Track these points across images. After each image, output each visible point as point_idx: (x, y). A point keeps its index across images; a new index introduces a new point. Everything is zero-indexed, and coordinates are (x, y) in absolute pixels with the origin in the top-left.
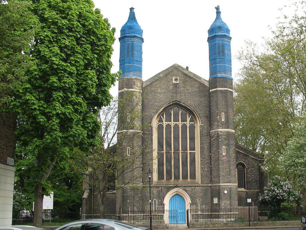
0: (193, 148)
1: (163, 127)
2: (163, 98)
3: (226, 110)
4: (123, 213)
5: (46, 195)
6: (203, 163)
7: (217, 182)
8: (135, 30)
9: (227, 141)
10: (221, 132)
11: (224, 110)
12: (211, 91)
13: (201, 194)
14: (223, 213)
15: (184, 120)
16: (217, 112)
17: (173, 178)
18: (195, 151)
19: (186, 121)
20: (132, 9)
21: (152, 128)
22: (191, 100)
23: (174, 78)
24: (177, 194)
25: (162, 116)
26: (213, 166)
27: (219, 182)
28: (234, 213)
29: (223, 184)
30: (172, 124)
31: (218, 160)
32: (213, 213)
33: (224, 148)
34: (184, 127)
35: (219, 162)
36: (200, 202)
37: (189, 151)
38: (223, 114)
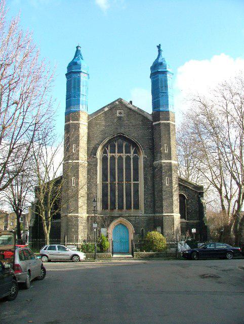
0: (136, 178)
19: (130, 153)
22: (134, 134)
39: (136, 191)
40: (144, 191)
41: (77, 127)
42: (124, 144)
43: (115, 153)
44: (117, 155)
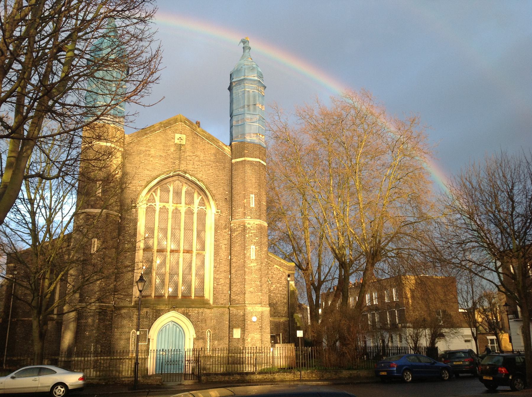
2: (157, 165)
4: (78, 354)
11: (254, 191)
15: (190, 202)
25: (154, 192)
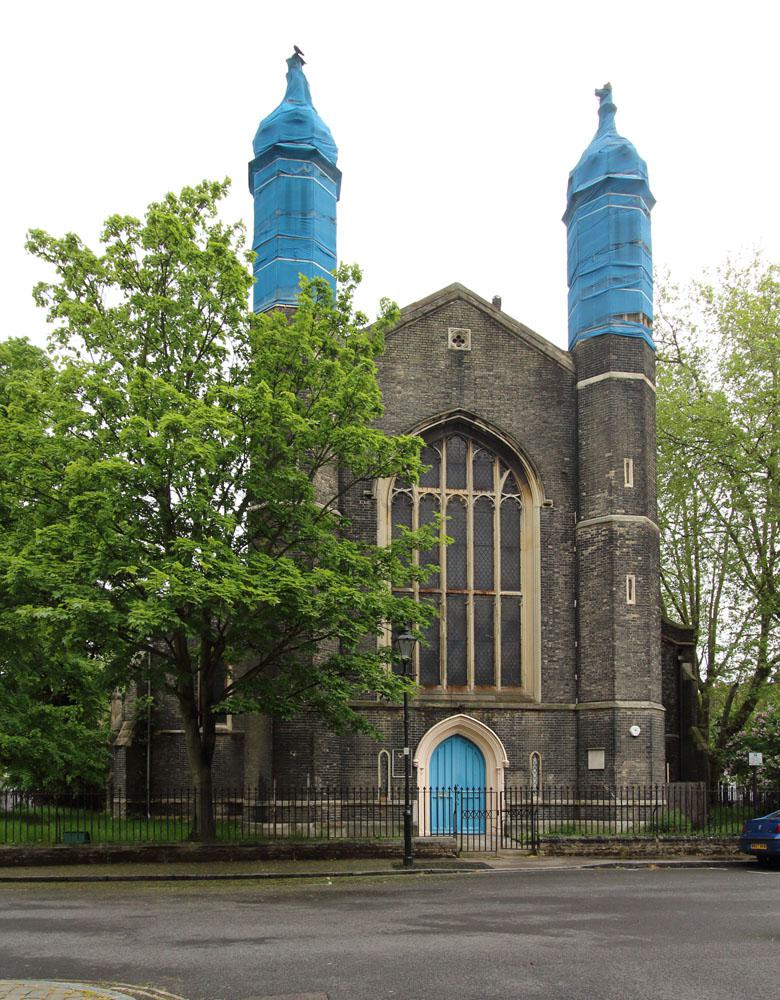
0: (513, 581)
1: (412, 505)
3: (640, 450)
5: (489, 319)
6: (550, 632)
7: (603, 698)
8: (313, 130)
9: (640, 558)
10: (622, 525)
12: (581, 384)
13: (544, 738)
14: (624, 803)
16: (607, 455)
17: (445, 682)
18: (518, 593)
19: (491, 488)
20: (296, 61)
21: (374, 502)
22: (512, 416)
23: (451, 333)
24: (457, 736)
26: (586, 642)
27: (611, 698)
28: (648, 802)
29: (627, 704)
30: (444, 494)
31: (609, 621)
32: (583, 801)
33: (630, 581)
34: (485, 505)
35: (613, 630)
36: (538, 762)
37: (499, 592)
38: (628, 464)
39: (513, 626)
40: (544, 624)
41: (382, 765)
42: (471, 456)
43: (438, 486)
44: (444, 493)
